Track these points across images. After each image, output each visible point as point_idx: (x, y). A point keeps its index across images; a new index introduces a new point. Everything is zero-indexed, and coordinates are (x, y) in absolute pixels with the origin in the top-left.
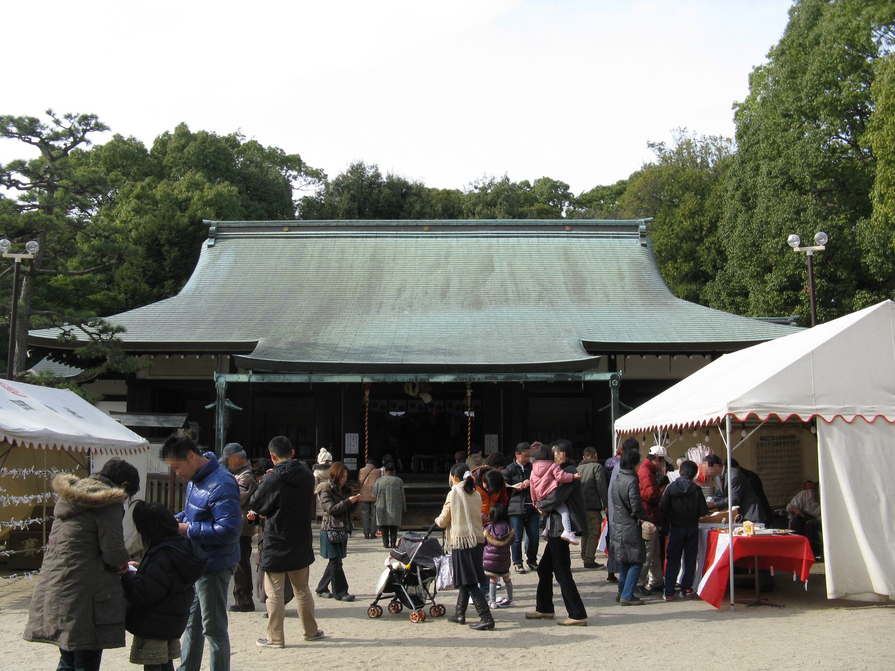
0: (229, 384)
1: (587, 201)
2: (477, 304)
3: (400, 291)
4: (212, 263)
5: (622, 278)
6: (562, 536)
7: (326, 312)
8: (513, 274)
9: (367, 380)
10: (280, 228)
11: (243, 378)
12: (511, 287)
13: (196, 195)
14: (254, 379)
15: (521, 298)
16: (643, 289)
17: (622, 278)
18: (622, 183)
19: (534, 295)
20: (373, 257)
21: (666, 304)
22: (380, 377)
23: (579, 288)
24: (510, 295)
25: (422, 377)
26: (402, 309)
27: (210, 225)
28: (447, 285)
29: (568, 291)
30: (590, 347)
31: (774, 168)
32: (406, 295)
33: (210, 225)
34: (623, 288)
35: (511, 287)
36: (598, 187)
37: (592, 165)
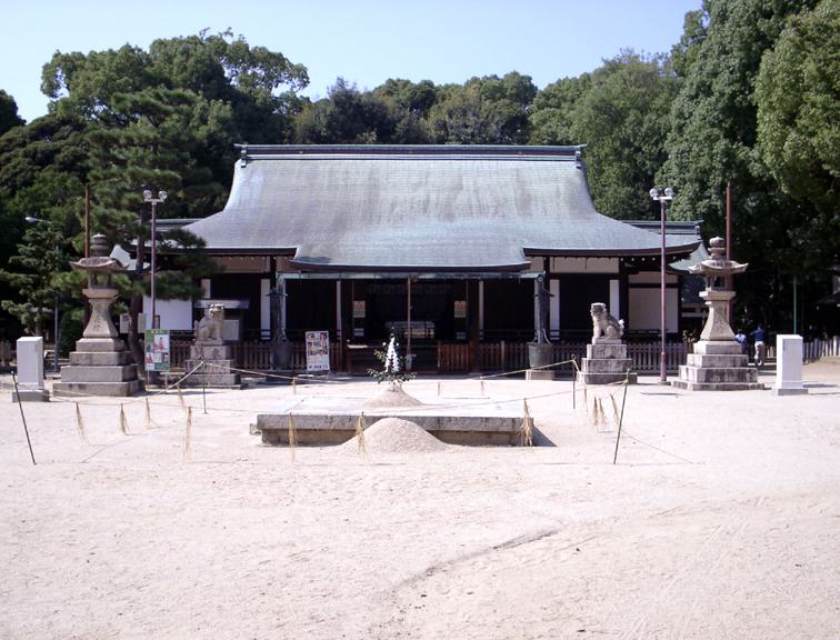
0: (288, 281)
1: (547, 95)
2: (450, 217)
3: (393, 206)
4: (247, 183)
5: (558, 196)
6: (457, 303)
7: (341, 224)
8: (476, 191)
9: (377, 277)
10: (297, 152)
11: (296, 276)
12: (474, 202)
13: (768, 577)
14: (303, 277)
15: (482, 210)
16: (573, 204)
17: (558, 196)
18: (586, 79)
19: (492, 210)
20: (372, 172)
21: (589, 218)
22: (386, 275)
23: (525, 203)
24: (474, 210)
25: (414, 274)
26: (395, 221)
27: (241, 149)
28: (427, 202)
29: (517, 206)
30: (529, 253)
31: (715, 74)
32: (398, 209)
33: (241, 149)
34: (558, 204)
35: (474, 202)
36: (560, 83)
37: (553, 61)
